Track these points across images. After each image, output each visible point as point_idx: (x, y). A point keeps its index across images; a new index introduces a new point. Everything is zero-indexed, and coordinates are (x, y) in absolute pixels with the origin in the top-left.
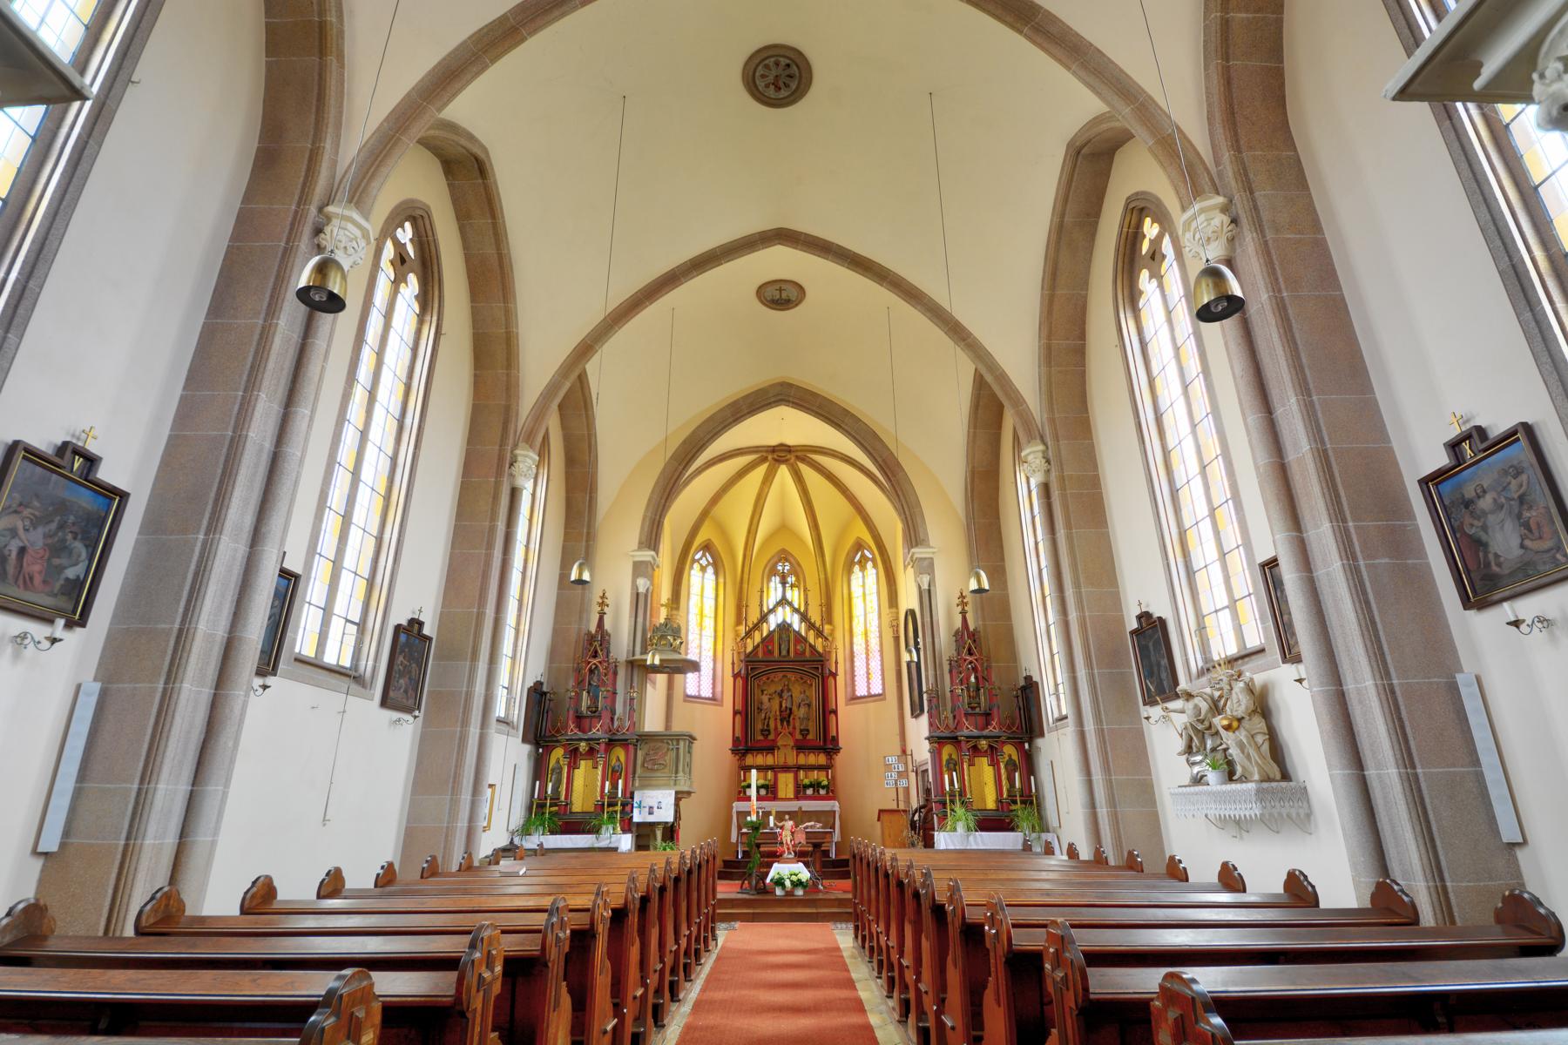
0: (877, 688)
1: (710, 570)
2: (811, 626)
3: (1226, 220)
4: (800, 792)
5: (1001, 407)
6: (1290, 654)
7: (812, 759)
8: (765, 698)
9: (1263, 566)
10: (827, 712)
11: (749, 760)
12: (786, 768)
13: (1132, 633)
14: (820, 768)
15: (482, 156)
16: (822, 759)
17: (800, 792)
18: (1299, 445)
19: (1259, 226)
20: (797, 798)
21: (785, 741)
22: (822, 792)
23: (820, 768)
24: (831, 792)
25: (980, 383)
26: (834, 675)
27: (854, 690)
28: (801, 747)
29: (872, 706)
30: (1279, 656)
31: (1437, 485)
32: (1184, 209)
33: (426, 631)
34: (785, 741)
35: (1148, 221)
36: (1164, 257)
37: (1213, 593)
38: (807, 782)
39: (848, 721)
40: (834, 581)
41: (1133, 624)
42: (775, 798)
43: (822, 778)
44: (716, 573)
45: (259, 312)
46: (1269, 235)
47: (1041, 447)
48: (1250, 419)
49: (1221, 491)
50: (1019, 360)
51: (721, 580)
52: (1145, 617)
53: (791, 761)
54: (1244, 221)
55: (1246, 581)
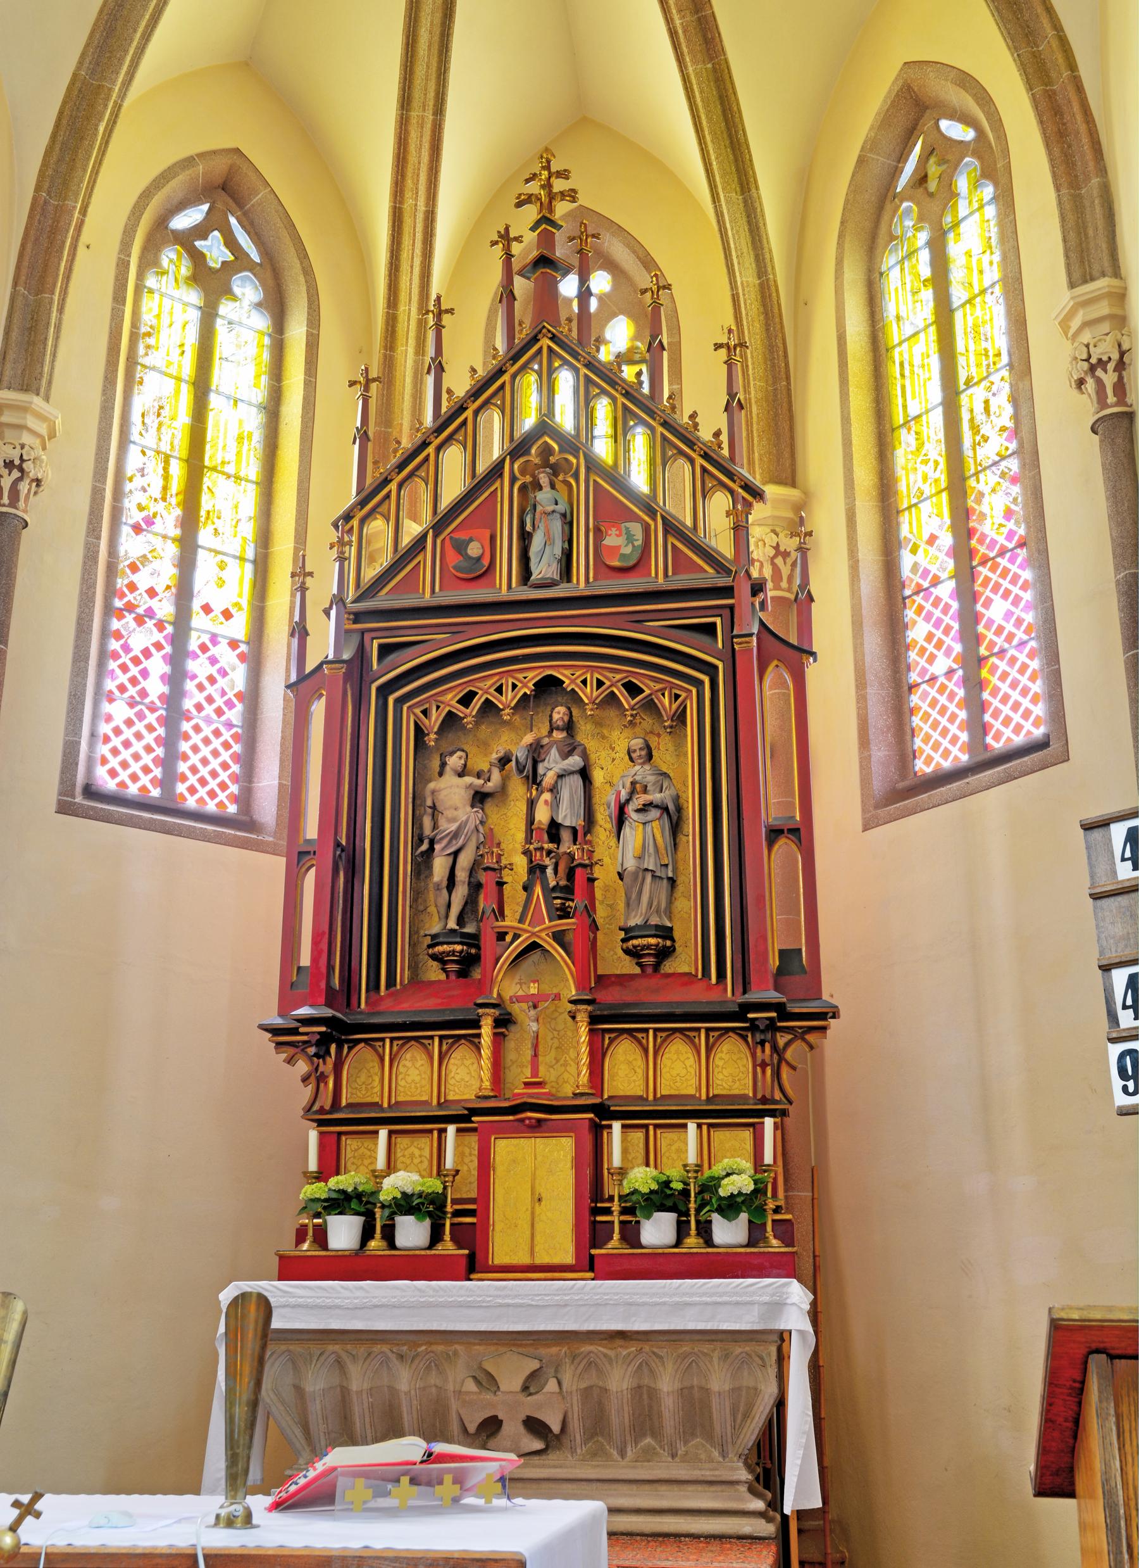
0: (1017, 719)
1: (247, 291)
2: (677, 439)
4: (603, 1237)
7: (680, 1070)
8: (452, 792)
10: (748, 828)
11: (366, 1078)
12: (532, 1114)
14: (718, 1113)
16: (733, 1069)
17: (603, 1237)
20: (589, 1264)
21: (543, 997)
22: (728, 1233)
23: (718, 1113)
24: (784, 1229)
26: (797, 655)
27: (904, 755)
28: (609, 1019)
29: (994, 802)
34: (543, 997)
38: (642, 1179)
39: (878, 896)
40: (803, 304)
42: (474, 1265)
43: (735, 1166)
44: (276, 306)
51: (297, 332)
53: (568, 1077)
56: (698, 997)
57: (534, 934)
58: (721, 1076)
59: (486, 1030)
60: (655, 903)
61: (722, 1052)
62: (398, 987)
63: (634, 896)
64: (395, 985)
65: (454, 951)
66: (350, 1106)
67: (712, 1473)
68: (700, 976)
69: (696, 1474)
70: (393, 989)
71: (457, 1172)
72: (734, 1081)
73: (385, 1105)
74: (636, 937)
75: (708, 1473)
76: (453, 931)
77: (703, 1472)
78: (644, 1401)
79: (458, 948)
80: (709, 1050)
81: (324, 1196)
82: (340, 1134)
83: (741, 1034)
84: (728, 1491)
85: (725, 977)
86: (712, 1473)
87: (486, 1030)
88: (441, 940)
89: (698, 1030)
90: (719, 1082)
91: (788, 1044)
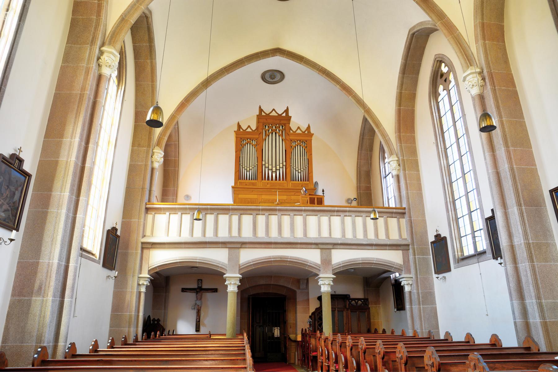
3: (480, 79)
5: (374, 132)
6: (496, 253)
9: (487, 219)
13: (432, 243)
15: (149, 15)
18: (504, 167)
19: (493, 84)
25: (365, 120)
30: (491, 256)
31: (555, 193)
32: (464, 72)
33: (119, 233)
35: (443, 65)
36: (450, 82)
37: (465, 229)
41: (432, 239)
45: (70, 104)
46: (511, 148)
47: (397, 159)
48: (490, 171)
49: (471, 185)
50: (386, 116)
52: (438, 236)
54: (487, 80)
55: (479, 224)
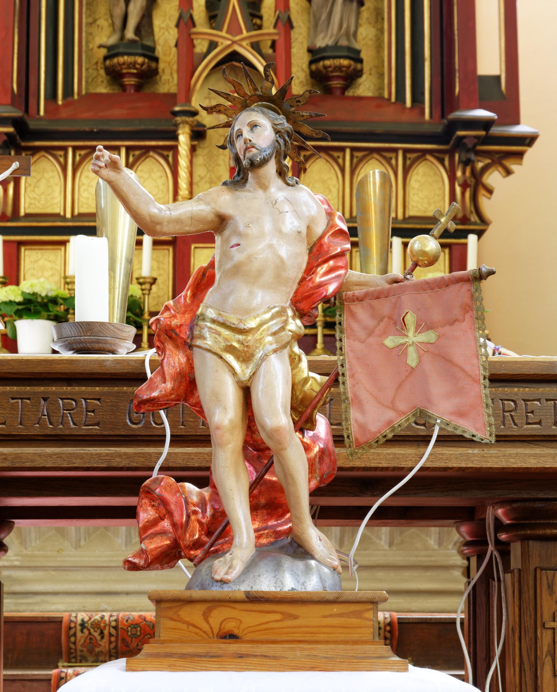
56: (388, 118)
57: (234, 42)
58: (416, 198)
59: (184, 139)
60: (345, 26)
61: (418, 174)
62: (76, 97)
63: (324, 17)
64: (72, 95)
65: (135, 63)
66: (28, 216)
67: (428, 559)
68: (393, 99)
69: (413, 560)
70: (70, 99)
71: (155, 280)
72: (429, 204)
73: (69, 215)
74: (328, 58)
75: (424, 559)
76: (132, 42)
77: (420, 559)
78: (71, 653)
79: (140, 60)
80: (406, 171)
81: (19, 299)
82: (20, 243)
83: (439, 156)
84: (444, 574)
85: (333, 140)
86: (428, 559)
87: (184, 139)
88: (121, 50)
89: (395, 150)
90: (415, 204)
91: (485, 169)
